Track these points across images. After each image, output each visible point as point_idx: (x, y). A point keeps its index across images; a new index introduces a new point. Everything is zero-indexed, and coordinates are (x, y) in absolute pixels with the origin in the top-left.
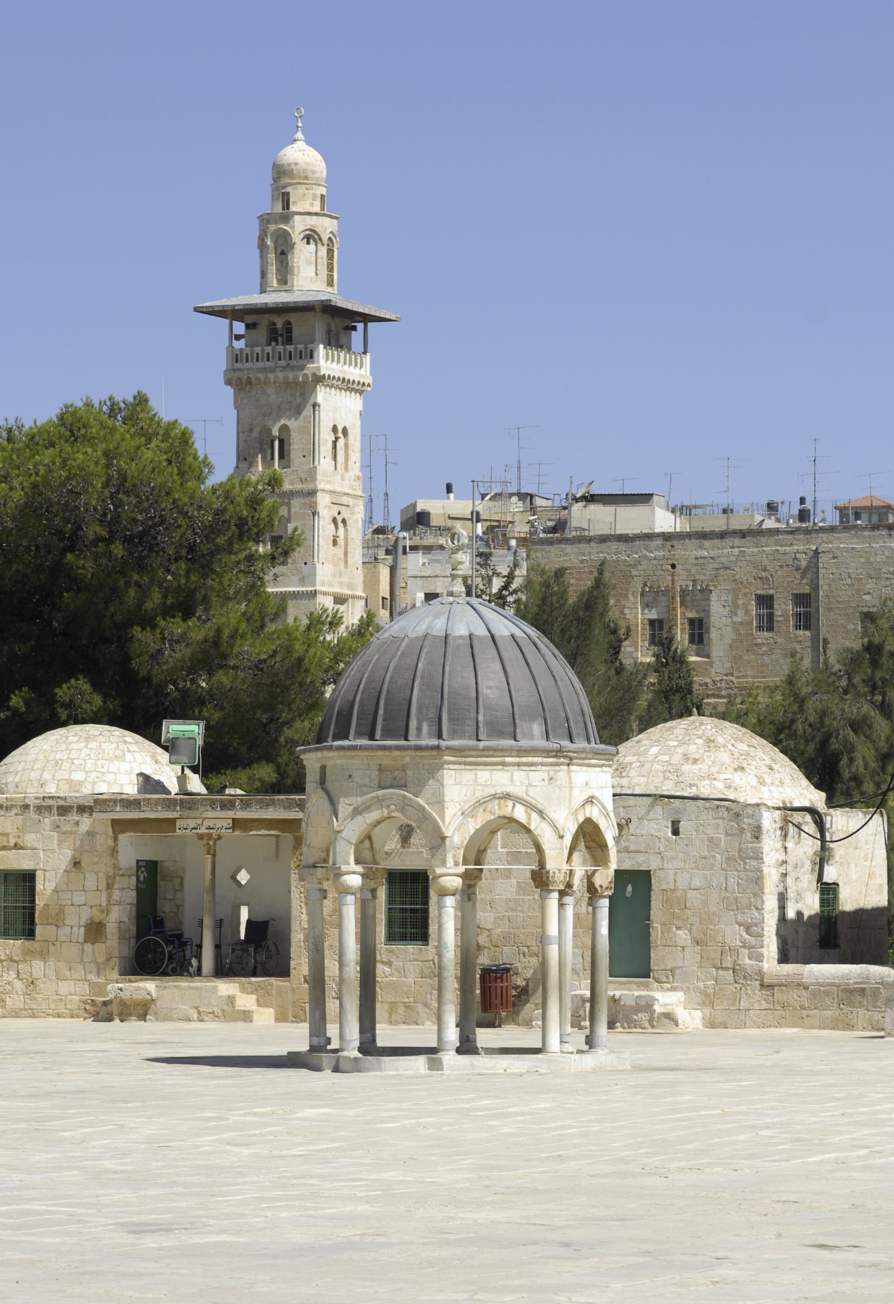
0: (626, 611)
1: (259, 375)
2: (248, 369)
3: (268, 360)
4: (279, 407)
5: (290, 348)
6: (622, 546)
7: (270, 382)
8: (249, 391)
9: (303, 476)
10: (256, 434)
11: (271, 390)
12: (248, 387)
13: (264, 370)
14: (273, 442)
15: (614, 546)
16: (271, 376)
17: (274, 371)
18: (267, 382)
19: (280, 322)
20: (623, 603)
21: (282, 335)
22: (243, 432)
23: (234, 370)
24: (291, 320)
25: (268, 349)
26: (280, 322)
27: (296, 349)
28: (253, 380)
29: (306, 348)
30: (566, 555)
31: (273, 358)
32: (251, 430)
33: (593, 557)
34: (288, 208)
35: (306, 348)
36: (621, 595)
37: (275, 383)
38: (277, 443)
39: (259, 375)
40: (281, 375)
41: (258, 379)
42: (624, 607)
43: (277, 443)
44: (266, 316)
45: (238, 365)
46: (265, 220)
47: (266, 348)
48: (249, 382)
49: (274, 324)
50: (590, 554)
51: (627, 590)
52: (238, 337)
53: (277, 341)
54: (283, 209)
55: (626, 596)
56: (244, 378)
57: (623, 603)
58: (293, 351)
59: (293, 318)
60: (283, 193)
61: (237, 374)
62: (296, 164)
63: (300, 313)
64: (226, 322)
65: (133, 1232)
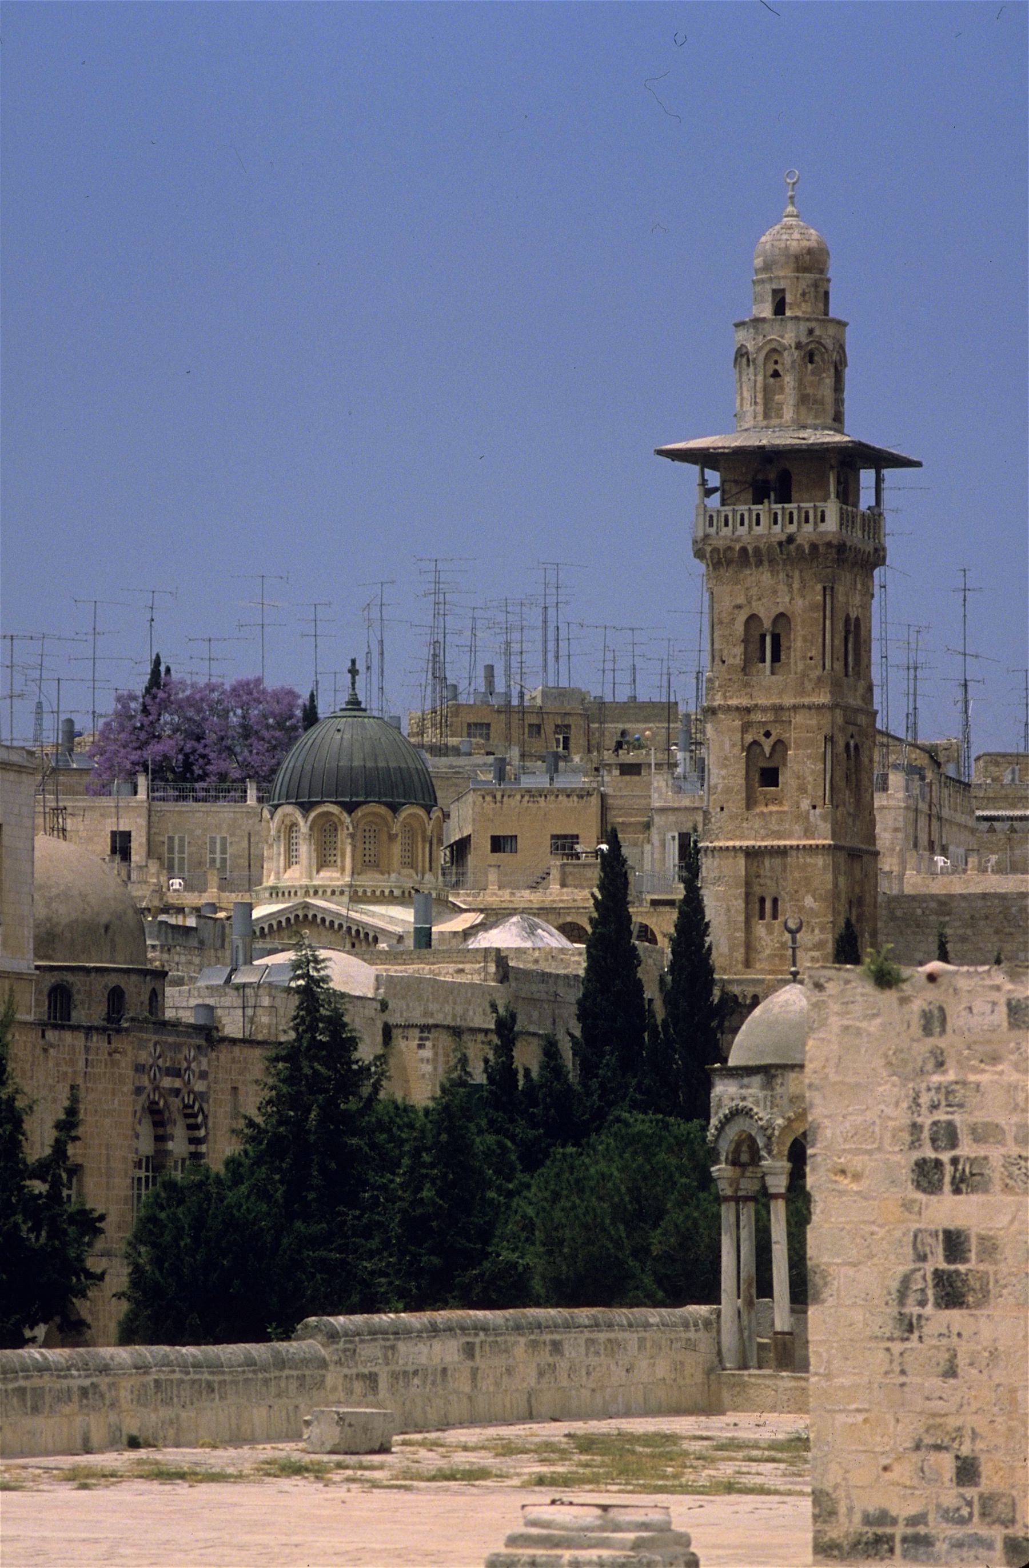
5: (791, 506)
14: (763, 637)
21: (775, 490)
43: (768, 639)
52: (709, 492)
53: (769, 497)
64: (696, 468)
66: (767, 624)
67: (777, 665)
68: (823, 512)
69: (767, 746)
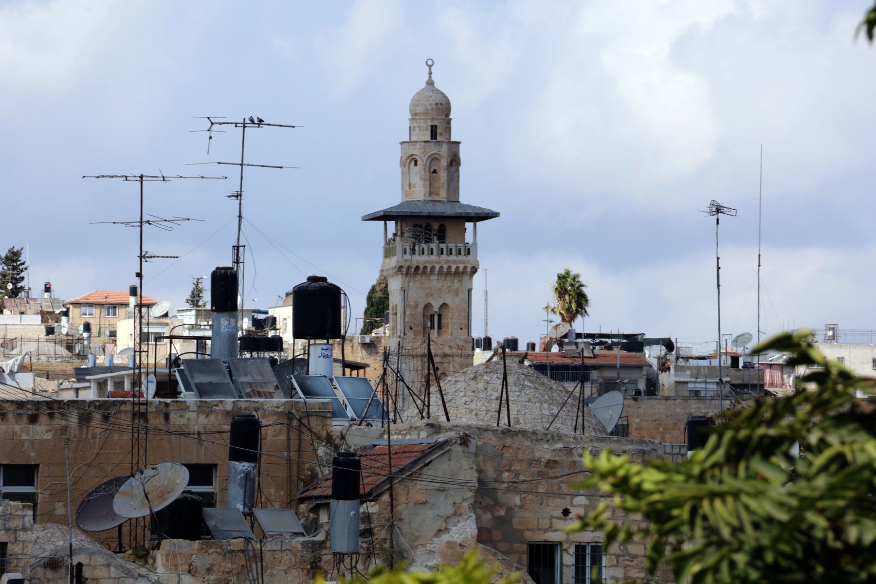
9: (461, 344)
66: (436, 308)
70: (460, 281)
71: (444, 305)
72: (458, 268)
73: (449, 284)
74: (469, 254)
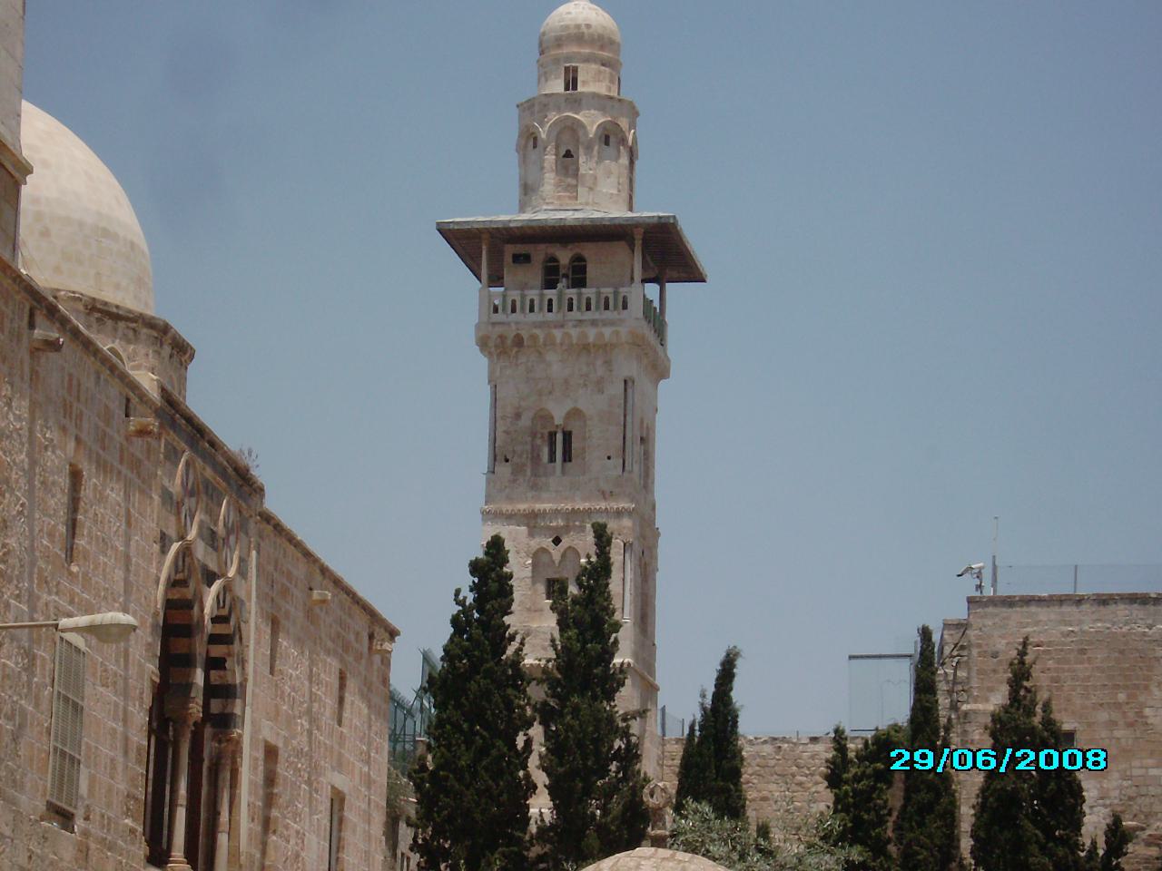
0: (1147, 711)
1: (537, 331)
2: (517, 323)
3: (550, 310)
4: (566, 381)
5: (588, 292)
6: (1137, 611)
7: (553, 344)
8: (516, 357)
10: (525, 421)
11: (551, 357)
12: (515, 349)
13: (541, 325)
15: (1122, 610)
16: (558, 334)
17: (562, 326)
18: (550, 342)
19: (564, 256)
20: (1142, 699)
21: (565, 276)
22: (504, 418)
23: (494, 324)
24: (586, 254)
25: (551, 293)
26: (564, 256)
27: (599, 294)
28: (525, 338)
29: (616, 294)
30: (1037, 623)
31: (560, 308)
32: (518, 416)
33: (1086, 628)
34: (575, 88)
35: (616, 294)
36: (1136, 687)
37: (561, 344)
38: (559, 437)
39: (537, 331)
40: (574, 332)
41: (534, 338)
42: (1142, 706)
43: (559, 437)
44: (542, 246)
45: (500, 317)
46: (532, 107)
47: (547, 292)
48: (519, 341)
49: (554, 259)
50: (1080, 622)
51: (1148, 679)
54: (567, 88)
55: (1146, 687)
56: (511, 335)
57: (1142, 699)
58: (575, 298)
59: (588, 250)
60: (567, 69)
61: (499, 330)
62: (588, 26)
63: (607, 245)
65: (218, 597)
67: (569, 464)
68: (625, 299)
69: (556, 553)
70: (608, 363)
71: (576, 413)
72: (601, 335)
73: (601, 371)
74: (625, 307)
